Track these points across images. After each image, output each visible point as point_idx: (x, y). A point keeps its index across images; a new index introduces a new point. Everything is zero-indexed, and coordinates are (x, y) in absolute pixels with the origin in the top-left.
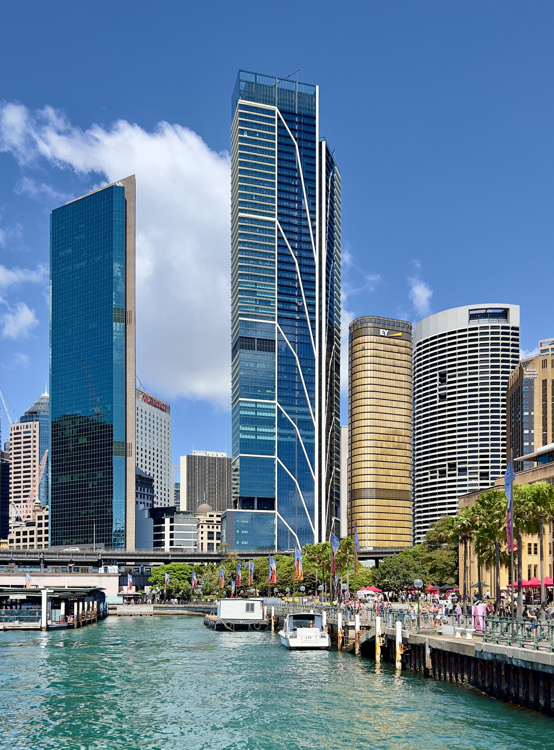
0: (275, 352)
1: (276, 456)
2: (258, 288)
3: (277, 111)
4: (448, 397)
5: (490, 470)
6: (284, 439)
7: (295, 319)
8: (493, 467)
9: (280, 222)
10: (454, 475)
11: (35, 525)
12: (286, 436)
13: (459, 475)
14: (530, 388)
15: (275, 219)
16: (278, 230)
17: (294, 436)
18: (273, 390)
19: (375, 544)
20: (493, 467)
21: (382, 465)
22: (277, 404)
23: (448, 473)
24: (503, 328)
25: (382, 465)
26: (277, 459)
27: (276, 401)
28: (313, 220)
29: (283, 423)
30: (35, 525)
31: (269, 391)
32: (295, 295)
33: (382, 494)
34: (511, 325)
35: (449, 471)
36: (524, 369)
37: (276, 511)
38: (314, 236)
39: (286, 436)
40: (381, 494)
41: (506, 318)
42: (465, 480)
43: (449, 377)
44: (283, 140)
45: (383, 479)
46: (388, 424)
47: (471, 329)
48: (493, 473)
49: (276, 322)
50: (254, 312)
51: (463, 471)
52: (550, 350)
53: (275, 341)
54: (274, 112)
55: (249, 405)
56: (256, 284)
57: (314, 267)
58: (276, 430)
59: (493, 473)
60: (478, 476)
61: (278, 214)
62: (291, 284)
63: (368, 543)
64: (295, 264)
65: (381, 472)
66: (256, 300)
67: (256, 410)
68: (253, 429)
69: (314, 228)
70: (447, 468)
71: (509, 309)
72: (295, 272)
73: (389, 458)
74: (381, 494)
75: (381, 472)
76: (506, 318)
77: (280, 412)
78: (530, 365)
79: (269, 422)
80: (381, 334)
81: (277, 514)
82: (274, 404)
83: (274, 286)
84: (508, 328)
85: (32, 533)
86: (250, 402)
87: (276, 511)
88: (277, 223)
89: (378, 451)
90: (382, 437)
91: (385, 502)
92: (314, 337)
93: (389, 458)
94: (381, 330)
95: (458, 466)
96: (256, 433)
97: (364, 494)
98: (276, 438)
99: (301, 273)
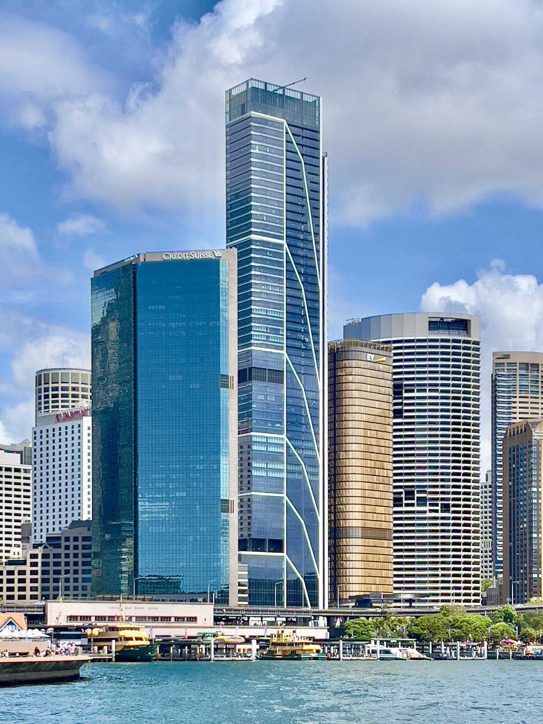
0: (283, 383)
1: (284, 495)
2: (269, 316)
3: (285, 124)
4: (405, 414)
5: (452, 503)
6: (292, 476)
7: (301, 349)
8: (454, 499)
9: (288, 245)
10: (412, 505)
11: (60, 547)
12: (293, 472)
13: (418, 505)
14: (538, 449)
15: (284, 242)
16: (287, 253)
17: (301, 473)
18: (281, 423)
19: (363, 588)
20: (454, 499)
21: (368, 501)
22: (286, 439)
23: (405, 502)
24: (465, 342)
25: (368, 501)
26: (286, 498)
27: (284, 436)
28: (317, 243)
29: (291, 460)
30: (60, 547)
31: (279, 425)
32: (301, 323)
33: (369, 533)
34: (472, 339)
35: (406, 499)
36: (533, 429)
37: (284, 554)
38: (318, 259)
39: (293, 472)
40: (368, 533)
41: (466, 330)
42: (425, 512)
43: (406, 391)
44: (291, 155)
45: (370, 517)
46: (374, 457)
47: (431, 340)
48: (454, 506)
49: (284, 352)
50: (264, 341)
51: (422, 501)
52: (506, 364)
53: (282, 372)
54: (283, 124)
55: (260, 440)
56: (267, 311)
57: (318, 293)
58: (284, 467)
59: (454, 506)
60: (439, 508)
61: (287, 236)
62: (297, 311)
63: (356, 587)
64: (301, 290)
65: (368, 508)
66: (267, 328)
67: (267, 444)
68: (263, 465)
69: (318, 251)
70: (403, 496)
71: (470, 320)
72: (302, 299)
73: (377, 494)
74: (368, 533)
75: (368, 508)
76: (466, 330)
77: (288, 447)
78: (538, 427)
79: (276, 458)
80: (369, 359)
81: (286, 557)
82: (283, 439)
83: (283, 313)
84: (468, 342)
85: (56, 556)
86: (262, 437)
87: (284, 554)
88: (286, 246)
89: (367, 486)
90: (369, 471)
91: (371, 542)
92: (318, 368)
93: (377, 494)
94: (368, 355)
95: (417, 495)
96: (267, 470)
97: (352, 533)
98: (284, 475)
99: (307, 299)
